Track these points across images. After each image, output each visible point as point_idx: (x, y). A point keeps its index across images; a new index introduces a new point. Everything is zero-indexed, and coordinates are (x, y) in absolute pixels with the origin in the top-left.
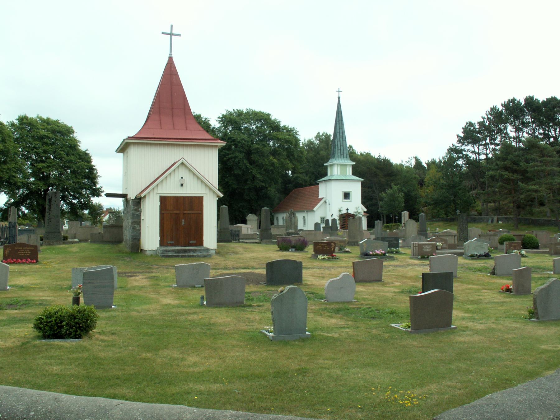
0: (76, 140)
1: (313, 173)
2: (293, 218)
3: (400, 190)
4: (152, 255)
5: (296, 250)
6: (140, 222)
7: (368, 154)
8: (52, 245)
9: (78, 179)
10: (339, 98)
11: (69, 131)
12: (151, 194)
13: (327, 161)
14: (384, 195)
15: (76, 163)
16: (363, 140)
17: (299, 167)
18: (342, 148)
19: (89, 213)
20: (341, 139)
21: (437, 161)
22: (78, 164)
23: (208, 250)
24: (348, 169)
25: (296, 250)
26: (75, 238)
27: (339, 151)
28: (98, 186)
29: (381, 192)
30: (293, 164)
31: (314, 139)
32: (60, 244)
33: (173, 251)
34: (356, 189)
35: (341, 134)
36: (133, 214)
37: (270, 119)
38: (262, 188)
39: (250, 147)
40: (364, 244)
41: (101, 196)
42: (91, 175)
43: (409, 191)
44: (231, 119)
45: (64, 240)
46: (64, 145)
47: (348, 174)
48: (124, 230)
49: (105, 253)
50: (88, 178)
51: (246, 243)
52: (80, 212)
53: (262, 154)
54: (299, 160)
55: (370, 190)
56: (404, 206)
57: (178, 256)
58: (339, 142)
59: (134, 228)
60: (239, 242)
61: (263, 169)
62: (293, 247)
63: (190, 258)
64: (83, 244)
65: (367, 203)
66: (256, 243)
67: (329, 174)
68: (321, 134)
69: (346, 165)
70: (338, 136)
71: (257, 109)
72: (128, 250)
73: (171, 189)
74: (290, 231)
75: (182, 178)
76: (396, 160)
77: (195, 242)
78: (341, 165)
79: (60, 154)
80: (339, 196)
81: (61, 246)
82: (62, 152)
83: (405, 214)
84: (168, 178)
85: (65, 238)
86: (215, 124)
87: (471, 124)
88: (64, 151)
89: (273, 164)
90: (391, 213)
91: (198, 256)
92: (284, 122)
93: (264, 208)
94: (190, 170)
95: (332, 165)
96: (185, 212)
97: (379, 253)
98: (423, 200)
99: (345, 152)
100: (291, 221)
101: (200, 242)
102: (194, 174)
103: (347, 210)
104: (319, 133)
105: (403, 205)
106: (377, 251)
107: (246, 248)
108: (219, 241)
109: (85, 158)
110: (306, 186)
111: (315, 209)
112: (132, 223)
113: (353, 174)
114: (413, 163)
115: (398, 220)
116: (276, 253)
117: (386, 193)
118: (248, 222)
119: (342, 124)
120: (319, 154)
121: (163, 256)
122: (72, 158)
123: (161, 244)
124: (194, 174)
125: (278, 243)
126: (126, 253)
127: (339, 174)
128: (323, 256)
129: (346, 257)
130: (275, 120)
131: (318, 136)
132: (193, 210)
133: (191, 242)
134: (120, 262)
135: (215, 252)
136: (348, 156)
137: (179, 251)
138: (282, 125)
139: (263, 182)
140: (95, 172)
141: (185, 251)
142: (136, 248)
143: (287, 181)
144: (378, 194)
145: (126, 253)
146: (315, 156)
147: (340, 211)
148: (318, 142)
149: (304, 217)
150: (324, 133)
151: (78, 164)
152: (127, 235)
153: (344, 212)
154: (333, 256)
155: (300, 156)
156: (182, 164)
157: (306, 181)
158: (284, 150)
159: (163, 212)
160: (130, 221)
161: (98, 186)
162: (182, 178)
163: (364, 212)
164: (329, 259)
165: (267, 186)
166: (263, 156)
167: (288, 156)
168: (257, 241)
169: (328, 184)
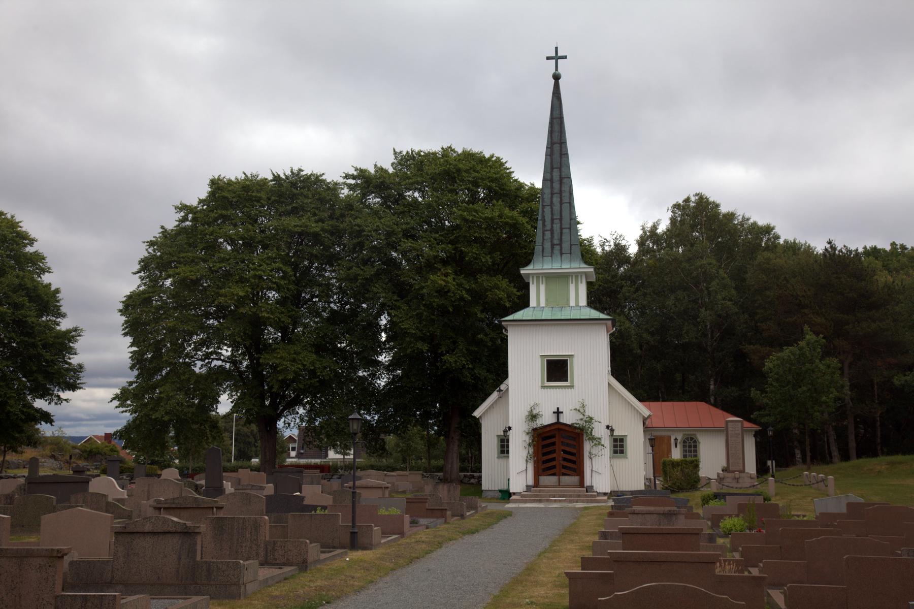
10: (557, 77)
13: (527, 263)
18: (557, 227)
20: (556, 200)
24: (572, 287)
27: (548, 234)
35: (556, 185)
47: (572, 303)
58: (548, 210)
67: (533, 302)
69: (564, 277)
87: (773, 228)
127: (543, 304)
147: (533, 417)
153: (547, 419)
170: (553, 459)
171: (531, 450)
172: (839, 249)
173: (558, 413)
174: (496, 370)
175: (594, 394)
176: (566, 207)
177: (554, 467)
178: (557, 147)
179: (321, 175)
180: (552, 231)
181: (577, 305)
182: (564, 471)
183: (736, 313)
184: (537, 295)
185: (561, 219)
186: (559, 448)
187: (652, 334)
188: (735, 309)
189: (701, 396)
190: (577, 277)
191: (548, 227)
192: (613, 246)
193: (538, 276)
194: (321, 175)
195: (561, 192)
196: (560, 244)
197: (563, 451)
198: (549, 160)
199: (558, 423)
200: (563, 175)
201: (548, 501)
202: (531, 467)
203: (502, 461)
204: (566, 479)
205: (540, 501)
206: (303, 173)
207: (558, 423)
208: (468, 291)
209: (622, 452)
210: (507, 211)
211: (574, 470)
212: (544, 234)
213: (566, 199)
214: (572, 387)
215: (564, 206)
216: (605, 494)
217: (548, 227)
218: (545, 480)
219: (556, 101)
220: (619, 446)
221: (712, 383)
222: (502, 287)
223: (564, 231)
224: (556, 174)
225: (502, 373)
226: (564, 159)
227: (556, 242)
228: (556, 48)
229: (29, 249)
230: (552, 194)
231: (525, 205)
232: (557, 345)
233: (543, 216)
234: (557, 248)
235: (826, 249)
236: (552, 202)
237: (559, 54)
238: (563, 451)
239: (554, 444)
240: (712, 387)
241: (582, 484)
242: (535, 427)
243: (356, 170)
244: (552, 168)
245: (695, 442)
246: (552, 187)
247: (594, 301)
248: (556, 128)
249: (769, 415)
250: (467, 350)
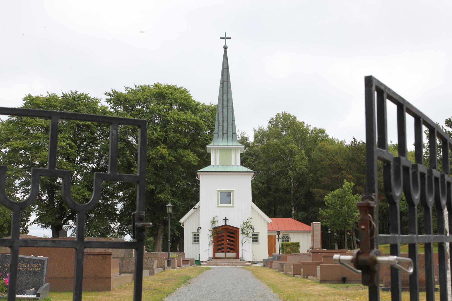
10: (225, 48)
18: (225, 124)
20: (225, 110)
21: (266, 129)
24: (233, 155)
27: (221, 128)
35: (225, 103)
47: (233, 163)
58: (221, 115)
69: (229, 150)
78: (221, 150)
80: (224, 195)
89: (162, 157)
103: (226, 220)
113: (242, 164)
127: (218, 163)
132: (89, 201)
147: (214, 222)
150: (278, 115)
153: (221, 223)
170: (223, 244)
171: (212, 239)
172: (358, 141)
174: (190, 198)
175: (243, 211)
176: (230, 114)
177: (223, 248)
178: (225, 83)
179: (87, 95)
180: (223, 126)
181: (236, 165)
182: (228, 250)
183: (307, 173)
184: (215, 158)
185: (227, 120)
186: (226, 239)
187: (263, 184)
188: (307, 171)
189: (287, 215)
190: (236, 150)
191: (221, 124)
192: (240, 138)
193: (215, 149)
194: (87, 95)
195: (227, 106)
196: (227, 133)
197: (228, 239)
198: (222, 90)
199: (226, 225)
200: (229, 98)
201: (221, 265)
202: (211, 248)
203: (196, 246)
204: (229, 254)
205: (217, 265)
206: (77, 93)
207: (226, 225)
208: (174, 157)
209: (257, 241)
210: (193, 116)
211: (233, 249)
212: (218, 128)
213: (230, 110)
214: (233, 206)
215: (229, 113)
216: (249, 262)
217: (221, 124)
218: (218, 255)
219: (225, 61)
220: (255, 238)
221: (293, 209)
222: (191, 157)
223: (229, 126)
224: (225, 97)
225: (196, 198)
226: (229, 89)
227: (225, 132)
228: (226, 33)
229: (183, 89)
230: (223, 107)
231: (201, 114)
232: (226, 183)
233: (218, 118)
234: (225, 135)
235: (352, 142)
236: (223, 111)
237: (224, 36)
238: (228, 239)
240: (293, 212)
241: (237, 257)
243: (126, 88)
244: (223, 94)
245: (288, 238)
246: (223, 104)
247: (243, 163)
248: (225, 73)
249: (328, 222)
250: (171, 190)
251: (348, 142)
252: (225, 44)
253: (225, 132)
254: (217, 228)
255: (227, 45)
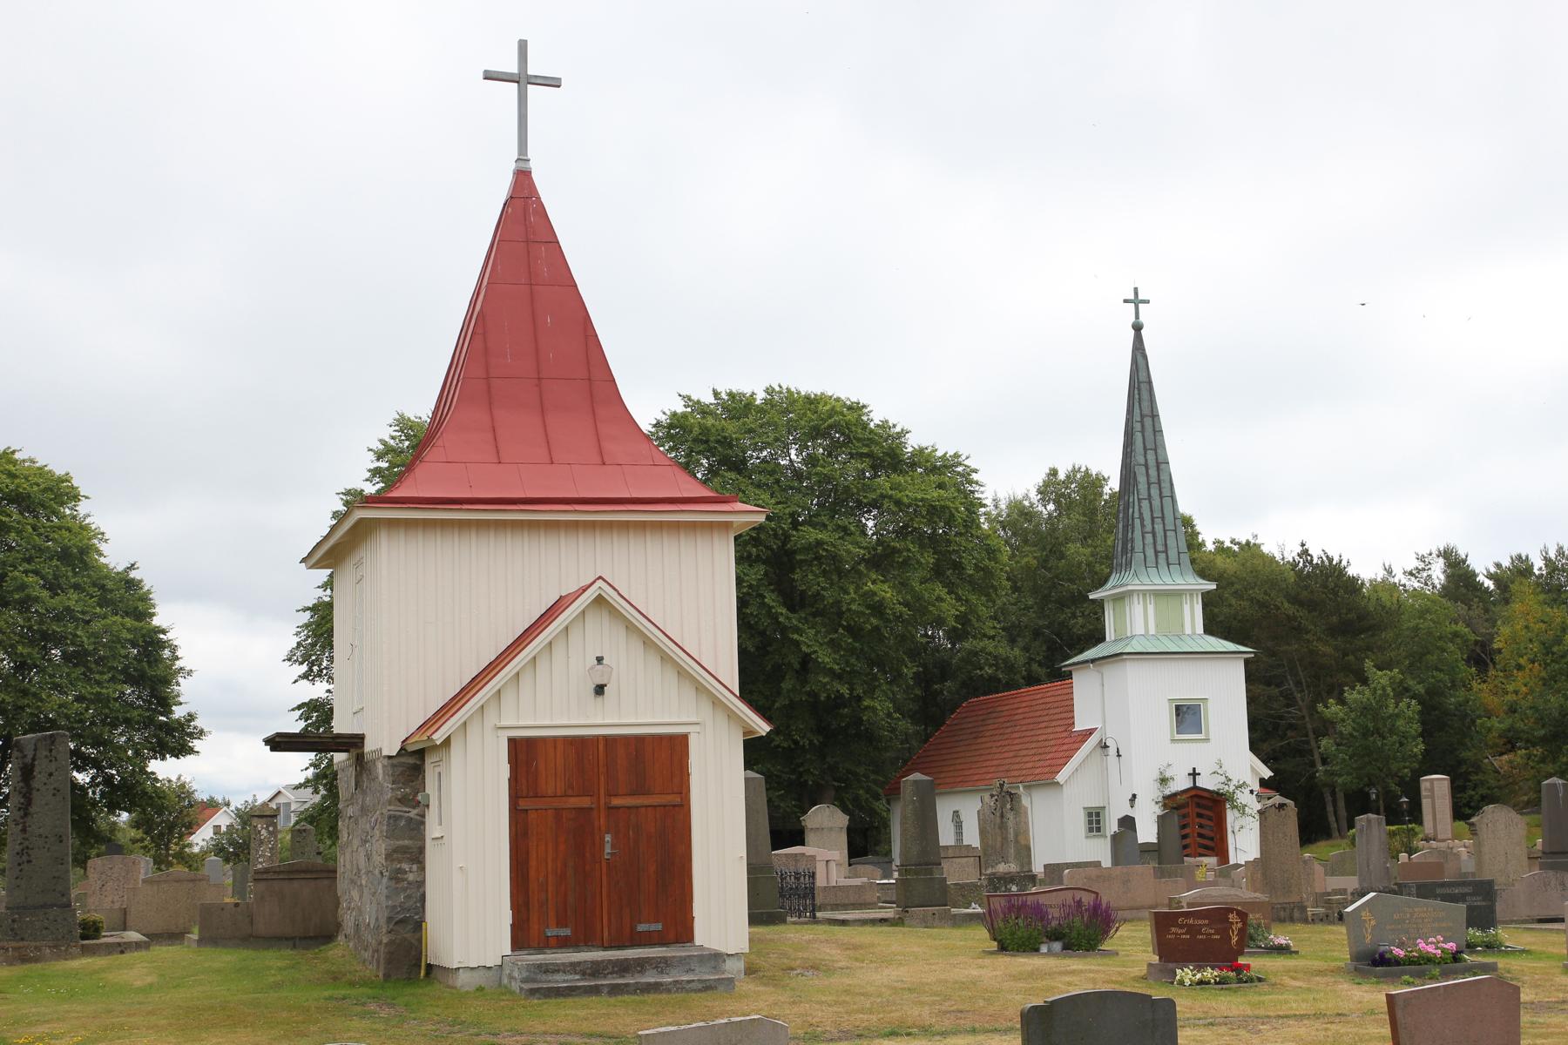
0: (85, 528)
1: (1037, 634)
2: (1010, 816)
3: (1402, 691)
4: (480, 989)
5: (1065, 948)
6: (422, 850)
7: (1250, 548)
8: (36, 960)
9: (99, 683)
10: (1138, 328)
11: (60, 492)
12: (473, 730)
14: (1333, 709)
15: (88, 622)
16: (1261, 492)
17: (983, 611)
19: (136, 825)
20: (1155, 492)
22: (97, 626)
23: (717, 958)
24: (1187, 608)
25: (1065, 948)
26: (125, 927)
27: (1149, 537)
28: (179, 712)
29: (1319, 697)
30: (959, 599)
31: (1034, 496)
32: (68, 956)
33: (574, 967)
34: (1225, 689)
35: (1153, 472)
36: (393, 819)
37: (865, 426)
38: (838, 702)
39: (787, 537)
40: (1365, 915)
41: (191, 751)
42: (150, 666)
43: (1433, 692)
44: (705, 430)
45: (84, 937)
46: (40, 550)
47: (1188, 631)
48: (342, 885)
49: (277, 986)
50: (136, 680)
51: (844, 923)
52: (102, 820)
53: (833, 566)
54: (983, 584)
55: (1275, 691)
56: (1426, 753)
57: (595, 990)
58: (1145, 504)
59: (397, 876)
60: (814, 920)
61: (896, 623)
62: (1054, 936)
63: (649, 998)
64: (163, 952)
65: (1265, 746)
66: (883, 921)
67: (1110, 634)
68: (1062, 476)
69: (1177, 594)
70: (1142, 479)
71: (808, 383)
72: (372, 971)
73: (555, 705)
74: (1002, 868)
75: (600, 660)
76: (1364, 569)
77: (659, 927)
78: (1158, 594)
79: (23, 587)
80: (1156, 719)
81: (75, 964)
82: (31, 579)
83: (1436, 787)
84: (542, 665)
85: (91, 930)
86: (370, 489)
87: (75, 497)
88: (36, 573)
89: (878, 608)
90: (1371, 784)
91: (678, 986)
92: (923, 432)
93: (911, 777)
94: (630, 627)
95: (1119, 598)
96: (616, 802)
97: (1431, 949)
98: (1498, 724)
99: (1171, 542)
100: (1003, 826)
101: (682, 930)
102: (648, 643)
103: (1194, 774)
104: (1054, 472)
105: (1419, 748)
106: (1422, 944)
107: (856, 947)
108: (754, 920)
109: (127, 598)
110: (1010, 686)
111: (1060, 778)
112: (388, 857)
113: (1208, 630)
114: (1438, 573)
115: (1410, 813)
116: (987, 961)
117: (1342, 701)
118: (809, 837)
119: (1157, 431)
120: (1062, 556)
121: (533, 992)
122: (72, 599)
123: (521, 939)
124: (648, 643)
125: (988, 919)
126: (365, 983)
127: (1152, 631)
128: (1199, 968)
129: (1292, 973)
130: (884, 425)
131: (1051, 487)
133: (641, 928)
134: (356, 1023)
135: (741, 965)
136: (1185, 558)
137: (596, 969)
138: (912, 442)
139: (838, 677)
140: (166, 653)
141: (624, 967)
142: (407, 959)
143: (935, 671)
144: (1312, 708)
145: (365, 983)
146: (1044, 564)
147: (1164, 781)
148: (1051, 507)
149: (956, 813)
150: (1075, 471)
151: (97, 626)
152: (363, 904)
153: (1181, 783)
154: (1238, 969)
155: (985, 570)
156: (600, 601)
157: (1010, 667)
158: (922, 546)
159: (523, 804)
160: (380, 847)
161: (179, 712)
162: (600, 660)
163: (1263, 783)
164: (1222, 982)
165: (859, 691)
166: (841, 573)
167: (938, 572)
168: (889, 913)
169: (1111, 672)
173: (1194, 774)
176: (1167, 501)
182: (1201, 851)
185: (1163, 518)
191: (1149, 528)
195: (1159, 483)
196: (1166, 552)
199: (1195, 787)
207: (1195, 787)
213: (1166, 492)
214: (1207, 740)
217: (1149, 528)
227: (1160, 548)
232: (1187, 682)
234: (1162, 556)
239: (524, 981)
242: (1167, 792)
251: (1291, 553)
252: (1137, 316)
253: (1160, 548)
254: (1175, 795)
255: (1142, 319)
